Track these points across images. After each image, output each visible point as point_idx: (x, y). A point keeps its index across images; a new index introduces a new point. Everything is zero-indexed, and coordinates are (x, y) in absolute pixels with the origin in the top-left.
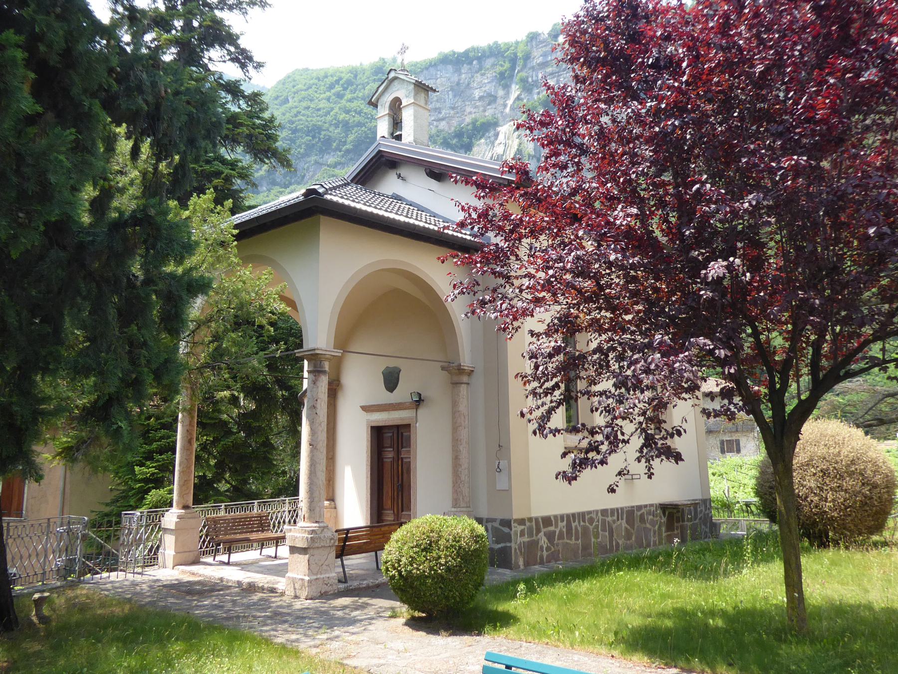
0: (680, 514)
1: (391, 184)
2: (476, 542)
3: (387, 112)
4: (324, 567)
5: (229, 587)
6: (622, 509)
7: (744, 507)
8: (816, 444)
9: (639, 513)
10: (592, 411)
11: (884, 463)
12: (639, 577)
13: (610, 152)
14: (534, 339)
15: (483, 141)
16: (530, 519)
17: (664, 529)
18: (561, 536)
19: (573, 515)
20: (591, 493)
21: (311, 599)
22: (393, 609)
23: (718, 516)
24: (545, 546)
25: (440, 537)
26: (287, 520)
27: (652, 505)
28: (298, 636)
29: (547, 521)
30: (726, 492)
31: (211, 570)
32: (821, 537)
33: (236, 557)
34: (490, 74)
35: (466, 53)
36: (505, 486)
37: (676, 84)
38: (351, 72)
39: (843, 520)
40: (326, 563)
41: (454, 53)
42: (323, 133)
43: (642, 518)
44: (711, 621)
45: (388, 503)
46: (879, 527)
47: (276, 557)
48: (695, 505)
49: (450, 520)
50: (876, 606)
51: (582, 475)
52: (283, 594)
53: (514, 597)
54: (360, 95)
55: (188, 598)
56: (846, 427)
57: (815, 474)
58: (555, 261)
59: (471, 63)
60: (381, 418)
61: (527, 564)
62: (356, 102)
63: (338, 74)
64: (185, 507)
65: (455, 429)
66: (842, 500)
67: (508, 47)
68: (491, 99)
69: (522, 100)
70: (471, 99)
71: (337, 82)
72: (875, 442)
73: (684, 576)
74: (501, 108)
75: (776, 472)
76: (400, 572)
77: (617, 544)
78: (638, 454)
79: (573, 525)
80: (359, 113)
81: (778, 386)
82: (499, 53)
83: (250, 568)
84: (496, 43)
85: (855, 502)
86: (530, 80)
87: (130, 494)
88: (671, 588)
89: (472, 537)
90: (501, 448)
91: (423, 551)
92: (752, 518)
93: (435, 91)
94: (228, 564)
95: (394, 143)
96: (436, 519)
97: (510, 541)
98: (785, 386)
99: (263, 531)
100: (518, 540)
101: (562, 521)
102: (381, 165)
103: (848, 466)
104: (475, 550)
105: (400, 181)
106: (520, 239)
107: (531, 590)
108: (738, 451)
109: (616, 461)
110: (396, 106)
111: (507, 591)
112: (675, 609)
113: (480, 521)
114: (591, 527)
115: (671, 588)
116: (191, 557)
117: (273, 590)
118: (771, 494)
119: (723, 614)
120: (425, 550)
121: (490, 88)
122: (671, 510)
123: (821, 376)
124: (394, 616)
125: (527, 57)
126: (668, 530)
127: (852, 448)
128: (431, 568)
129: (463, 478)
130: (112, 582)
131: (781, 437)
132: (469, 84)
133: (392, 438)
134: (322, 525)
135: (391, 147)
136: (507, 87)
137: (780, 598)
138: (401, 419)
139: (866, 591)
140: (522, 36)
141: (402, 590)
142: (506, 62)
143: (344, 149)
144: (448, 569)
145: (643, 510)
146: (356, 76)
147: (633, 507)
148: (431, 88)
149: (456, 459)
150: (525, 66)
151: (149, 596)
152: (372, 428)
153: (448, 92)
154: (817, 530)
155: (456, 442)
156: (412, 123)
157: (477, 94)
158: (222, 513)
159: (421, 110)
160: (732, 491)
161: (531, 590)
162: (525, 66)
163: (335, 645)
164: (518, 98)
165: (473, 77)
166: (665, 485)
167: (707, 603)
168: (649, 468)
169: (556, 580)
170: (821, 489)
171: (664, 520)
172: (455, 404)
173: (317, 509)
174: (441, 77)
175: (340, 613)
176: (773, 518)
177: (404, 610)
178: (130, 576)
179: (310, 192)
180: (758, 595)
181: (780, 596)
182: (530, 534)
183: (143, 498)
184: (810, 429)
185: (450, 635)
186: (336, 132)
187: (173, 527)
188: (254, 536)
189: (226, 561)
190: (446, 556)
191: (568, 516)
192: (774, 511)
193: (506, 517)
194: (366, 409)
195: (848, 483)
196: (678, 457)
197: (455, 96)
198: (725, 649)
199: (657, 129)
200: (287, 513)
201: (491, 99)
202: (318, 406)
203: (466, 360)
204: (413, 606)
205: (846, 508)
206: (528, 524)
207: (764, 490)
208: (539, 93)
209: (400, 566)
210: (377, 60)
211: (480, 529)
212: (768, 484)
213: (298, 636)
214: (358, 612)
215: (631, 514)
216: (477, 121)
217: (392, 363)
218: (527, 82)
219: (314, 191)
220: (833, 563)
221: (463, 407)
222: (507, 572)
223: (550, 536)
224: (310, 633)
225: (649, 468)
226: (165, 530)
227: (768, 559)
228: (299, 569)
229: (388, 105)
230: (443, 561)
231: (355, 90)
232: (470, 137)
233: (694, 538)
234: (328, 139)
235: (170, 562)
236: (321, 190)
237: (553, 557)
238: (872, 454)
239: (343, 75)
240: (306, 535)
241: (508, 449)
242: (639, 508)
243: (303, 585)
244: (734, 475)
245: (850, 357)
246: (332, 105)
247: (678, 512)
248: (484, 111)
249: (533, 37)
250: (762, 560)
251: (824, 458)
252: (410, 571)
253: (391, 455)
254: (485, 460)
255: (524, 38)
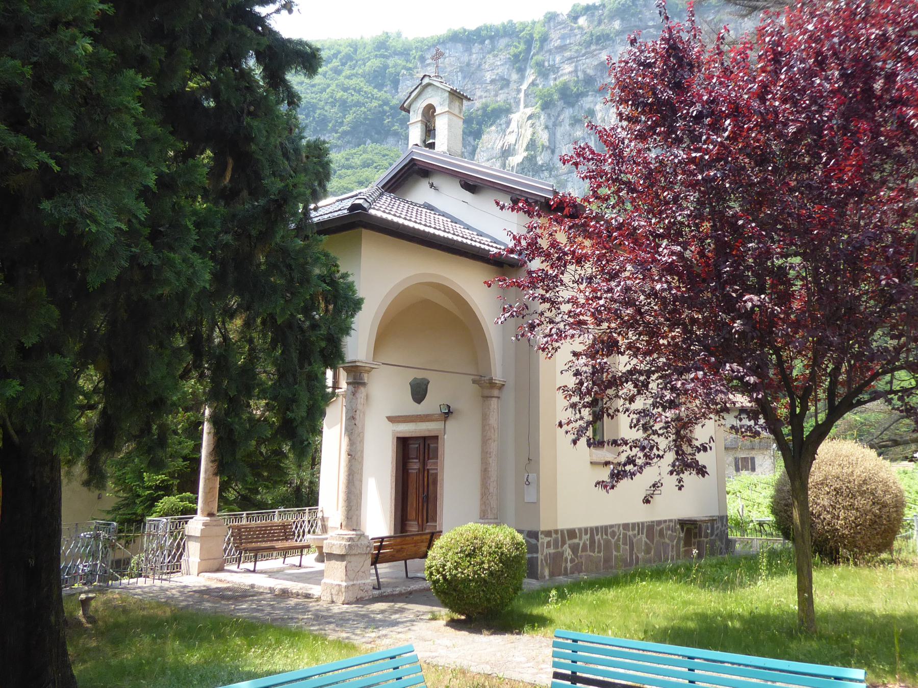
0: (697, 530)
1: (422, 193)
2: (517, 549)
3: (420, 119)
4: (360, 573)
5: (262, 593)
6: (643, 523)
7: (757, 527)
8: (831, 463)
9: (658, 528)
10: (631, 427)
11: (894, 483)
12: (660, 587)
13: (651, 187)
14: (574, 359)
15: (493, 128)
16: (556, 532)
17: (682, 543)
18: (584, 549)
19: (597, 528)
20: (624, 506)
21: (347, 604)
22: (432, 612)
23: (734, 535)
24: (569, 558)
25: (484, 543)
26: (306, 530)
27: (671, 521)
28: (348, 635)
29: (572, 533)
30: (740, 510)
31: (237, 577)
32: (831, 553)
33: (261, 565)
34: (504, 56)
35: (478, 31)
36: (533, 499)
37: (719, 140)
38: (350, 45)
39: (853, 537)
40: (362, 570)
41: (465, 31)
42: (318, 112)
43: (661, 532)
44: (730, 623)
45: (412, 513)
46: (886, 544)
47: (300, 566)
48: (712, 521)
49: (492, 528)
50: (877, 613)
51: (619, 485)
52: (318, 599)
53: (545, 602)
54: (360, 71)
55: (223, 602)
56: (860, 448)
57: (828, 493)
58: (607, 292)
59: (482, 42)
60: (407, 429)
61: (552, 575)
62: (355, 79)
63: (336, 47)
64: (210, 515)
65: (485, 441)
66: (853, 518)
67: (524, 26)
68: (505, 83)
69: (537, 85)
70: (482, 82)
71: (335, 56)
72: (887, 463)
73: (703, 586)
74: (514, 94)
75: (793, 489)
76: (444, 577)
77: (637, 558)
78: (671, 468)
79: (596, 538)
80: (359, 91)
81: (798, 410)
82: (513, 32)
83: (277, 576)
84: (511, 21)
85: (865, 521)
86: (546, 64)
87: (138, 501)
88: (691, 597)
89: (513, 544)
90: (530, 461)
91: (467, 556)
92: (764, 537)
93: (469, 99)
94: (254, 571)
95: (426, 152)
96: (463, 530)
97: (537, 552)
98: (805, 408)
99: (287, 539)
100: (545, 551)
101: (586, 534)
102: (412, 173)
103: (860, 485)
104: (515, 557)
105: (432, 190)
106: (565, 266)
107: (562, 596)
108: (753, 469)
109: (650, 475)
110: (429, 113)
111: (541, 597)
112: (696, 614)
113: (520, 531)
114: (613, 541)
115: (691, 597)
116: (216, 564)
117: (308, 596)
118: (786, 511)
119: (740, 617)
120: (469, 555)
121: (503, 70)
122: (689, 526)
123: (837, 403)
124: (434, 618)
125: (544, 39)
126: (685, 545)
127: (865, 468)
128: (475, 573)
129: (491, 490)
130: (139, 588)
131: (799, 455)
132: (480, 65)
133: (418, 449)
134: (358, 533)
135: (424, 156)
136: (521, 71)
137: (792, 606)
138: (429, 431)
139: (871, 601)
140: (539, 16)
141: (445, 593)
142: (524, 46)
143: (340, 130)
144: (491, 574)
145: (663, 525)
146: (356, 50)
147: (653, 522)
148: (466, 97)
149: (485, 472)
150: (541, 48)
151: (183, 601)
152: (398, 438)
153: (457, 72)
154: (828, 547)
155: (485, 455)
156: (446, 132)
157: (489, 76)
158: (244, 522)
159: (455, 118)
160: (746, 509)
161: (562, 596)
162: (541, 48)
163: (386, 641)
164: (533, 84)
165: (484, 57)
166: (681, 501)
167: (725, 609)
168: (680, 481)
169: (583, 588)
170: (834, 508)
171: (682, 535)
172: (485, 418)
173: (355, 518)
174: (450, 56)
175: (379, 616)
176: (786, 535)
177: (444, 613)
178: (158, 583)
179: (354, 207)
180: (771, 603)
181: (792, 603)
182: (556, 547)
183: (152, 506)
184: (825, 449)
185: (492, 634)
186: (332, 112)
187: (198, 534)
188: (279, 545)
189: (252, 569)
190: (489, 562)
191: (592, 529)
192: (789, 528)
193: (534, 528)
194: (392, 419)
195: (860, 502)
196: (702, 471)
197: (464, 78)
198: (743, 644)
199: (700, 177)
200: (306, 523)
201: (505, 83)
202: (357, 417)
203: (498, 375)
204: (453, 607)
205: (857, 526)
206: (554, 536)
207: (780, 508)
208: (555, 79)
209: (444, 570)
210: (380, 33)
211: (520, 538)
212: (783, 502)
213: (348, 635)
214: (397, 616)
215: (651, 529)
216: (487, 106)
217: (420, 375)
218: (544, 66)
219: (359, 206)
220: (842, 577)
221: (493, 420)
222: (534, 581)
223: (574, 548)
224: (358, 631)
225: (680, 481)
226: (189, 537)
227: (782, 572)
228: (335, 575)
229: (420, 111)
230: (486, 566)
231: (355, 66)
232: (480, 124)
233: (712, 554)
234: (323, 119)
235: (194, 569)
236: (366, 205)
237: (577, 568)
238: (883, 475)
239: (341, 49)
240: (344, 542)
241: (538, 462)
242: (659, 523)
243: (340, 590)
244: (750, 493)
245: (860, 390)
246: (328, 81)
247: (696, 528)
248: (496, 95)
249: (551, 18)
250: (775, 573)
251: (838, 478)
252: (455, 575)
253: (416, 466)
254: (514, 473)
255: (542, 18)
